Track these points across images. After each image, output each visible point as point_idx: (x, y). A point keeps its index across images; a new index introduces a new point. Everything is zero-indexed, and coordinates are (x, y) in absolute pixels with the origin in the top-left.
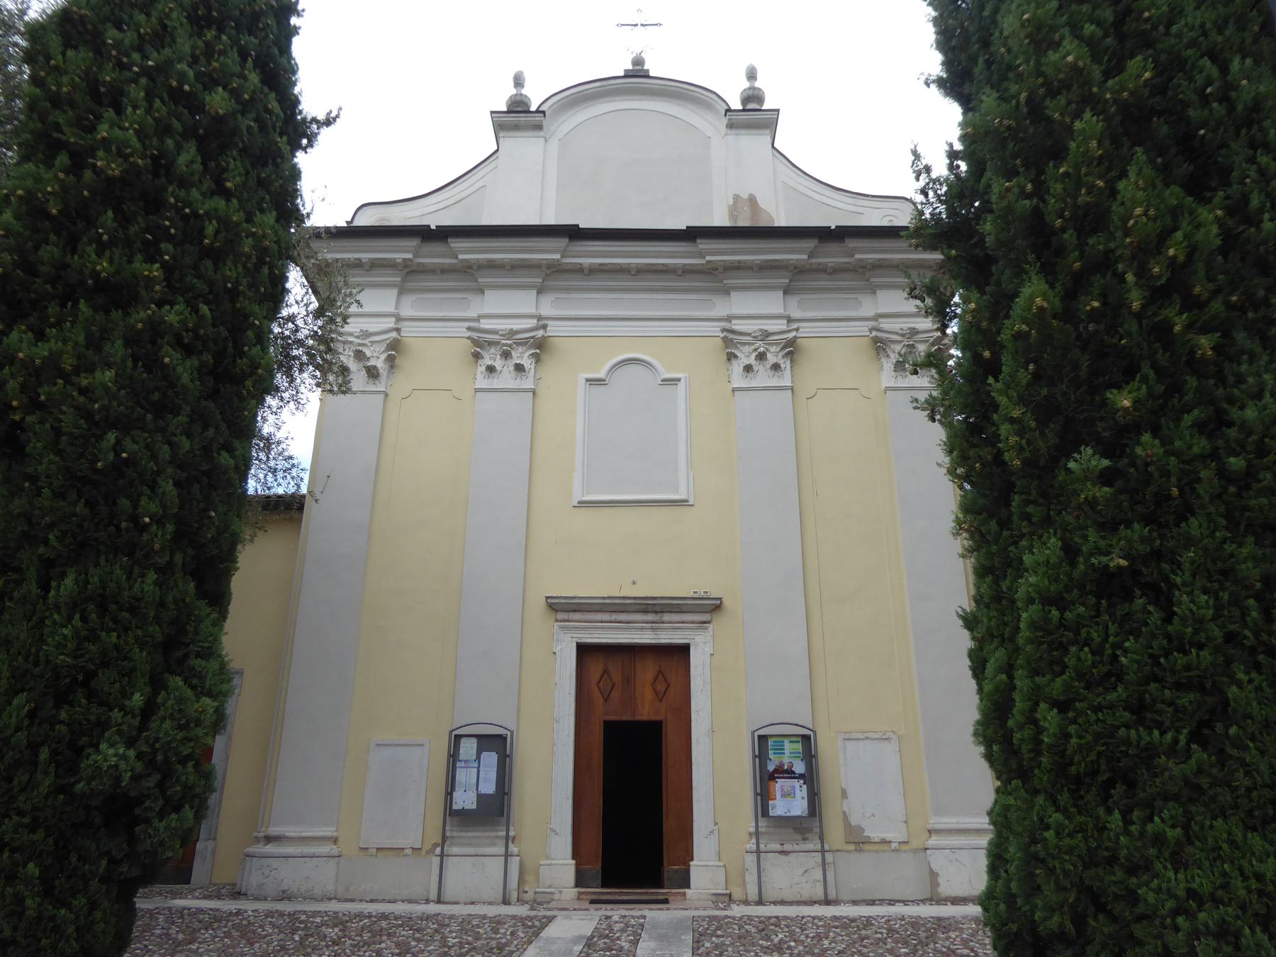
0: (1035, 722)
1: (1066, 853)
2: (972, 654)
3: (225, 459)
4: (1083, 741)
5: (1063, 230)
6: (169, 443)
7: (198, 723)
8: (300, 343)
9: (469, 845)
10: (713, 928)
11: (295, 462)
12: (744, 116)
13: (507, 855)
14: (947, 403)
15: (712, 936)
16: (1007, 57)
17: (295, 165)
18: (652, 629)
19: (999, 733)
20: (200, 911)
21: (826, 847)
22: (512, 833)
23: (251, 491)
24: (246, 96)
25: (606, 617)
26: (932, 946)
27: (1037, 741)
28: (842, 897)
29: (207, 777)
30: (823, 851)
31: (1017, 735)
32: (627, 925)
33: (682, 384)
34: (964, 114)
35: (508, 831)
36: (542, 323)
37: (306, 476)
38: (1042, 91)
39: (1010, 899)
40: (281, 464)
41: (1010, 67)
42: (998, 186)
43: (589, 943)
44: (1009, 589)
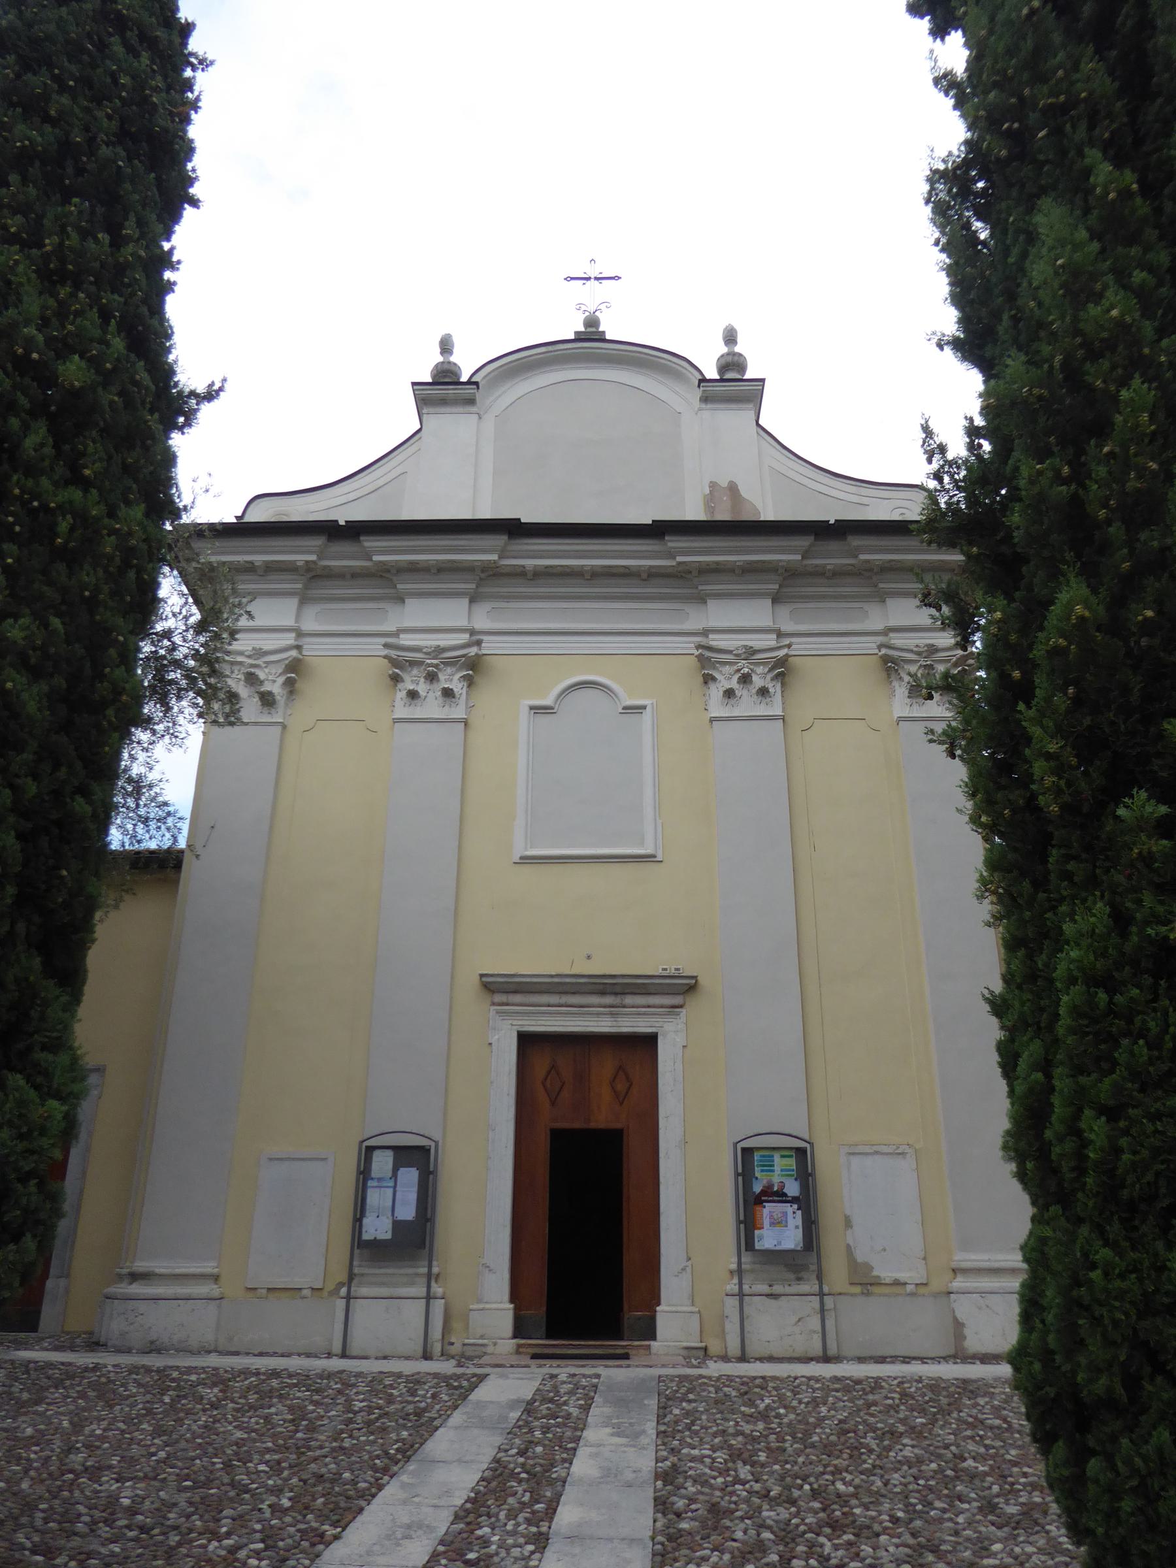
0: (1078, 1133)
1: (1116, 1298)
2: (1001, 1047)
3: (80, 805)
4: (1137, 1158)
5: (1109, 522)
6: (11, 786)
7: (43, 1131)
8: (177, 664)
9: (383, 1284)
10: (683, 1390)
11: (171, 809)
12: (721, 388)
13: (429, 1298)
14: (968, 734)
15: (682, 1400)
16: (1037, 312)
17: (169, 447)
18: (612, 1014)
19: (1035, 1145)
20: (50, 1365)
21: (826, 1289)
22: (435, 1270)
23: (115, 845)
24: (108, 365)
25: (554, 999)
26: (955, 1415)
27: (1080, 1156)
28: (846, 1352)
29: (55, 1198)
30: (821, 1294)
31: (1056, 1150)
32: (577, 1386)
33: (647, 715)
34: (985, 382)
35: (430, 1267)
36: (475, 638)
37: (185, 827)
38: (1080, 353)
39: (1047, 1355)
40: (154, 812)
41: (1041, 325)
42: (1028, 468)
43: (529, 1408)
44: (1046, 965)
